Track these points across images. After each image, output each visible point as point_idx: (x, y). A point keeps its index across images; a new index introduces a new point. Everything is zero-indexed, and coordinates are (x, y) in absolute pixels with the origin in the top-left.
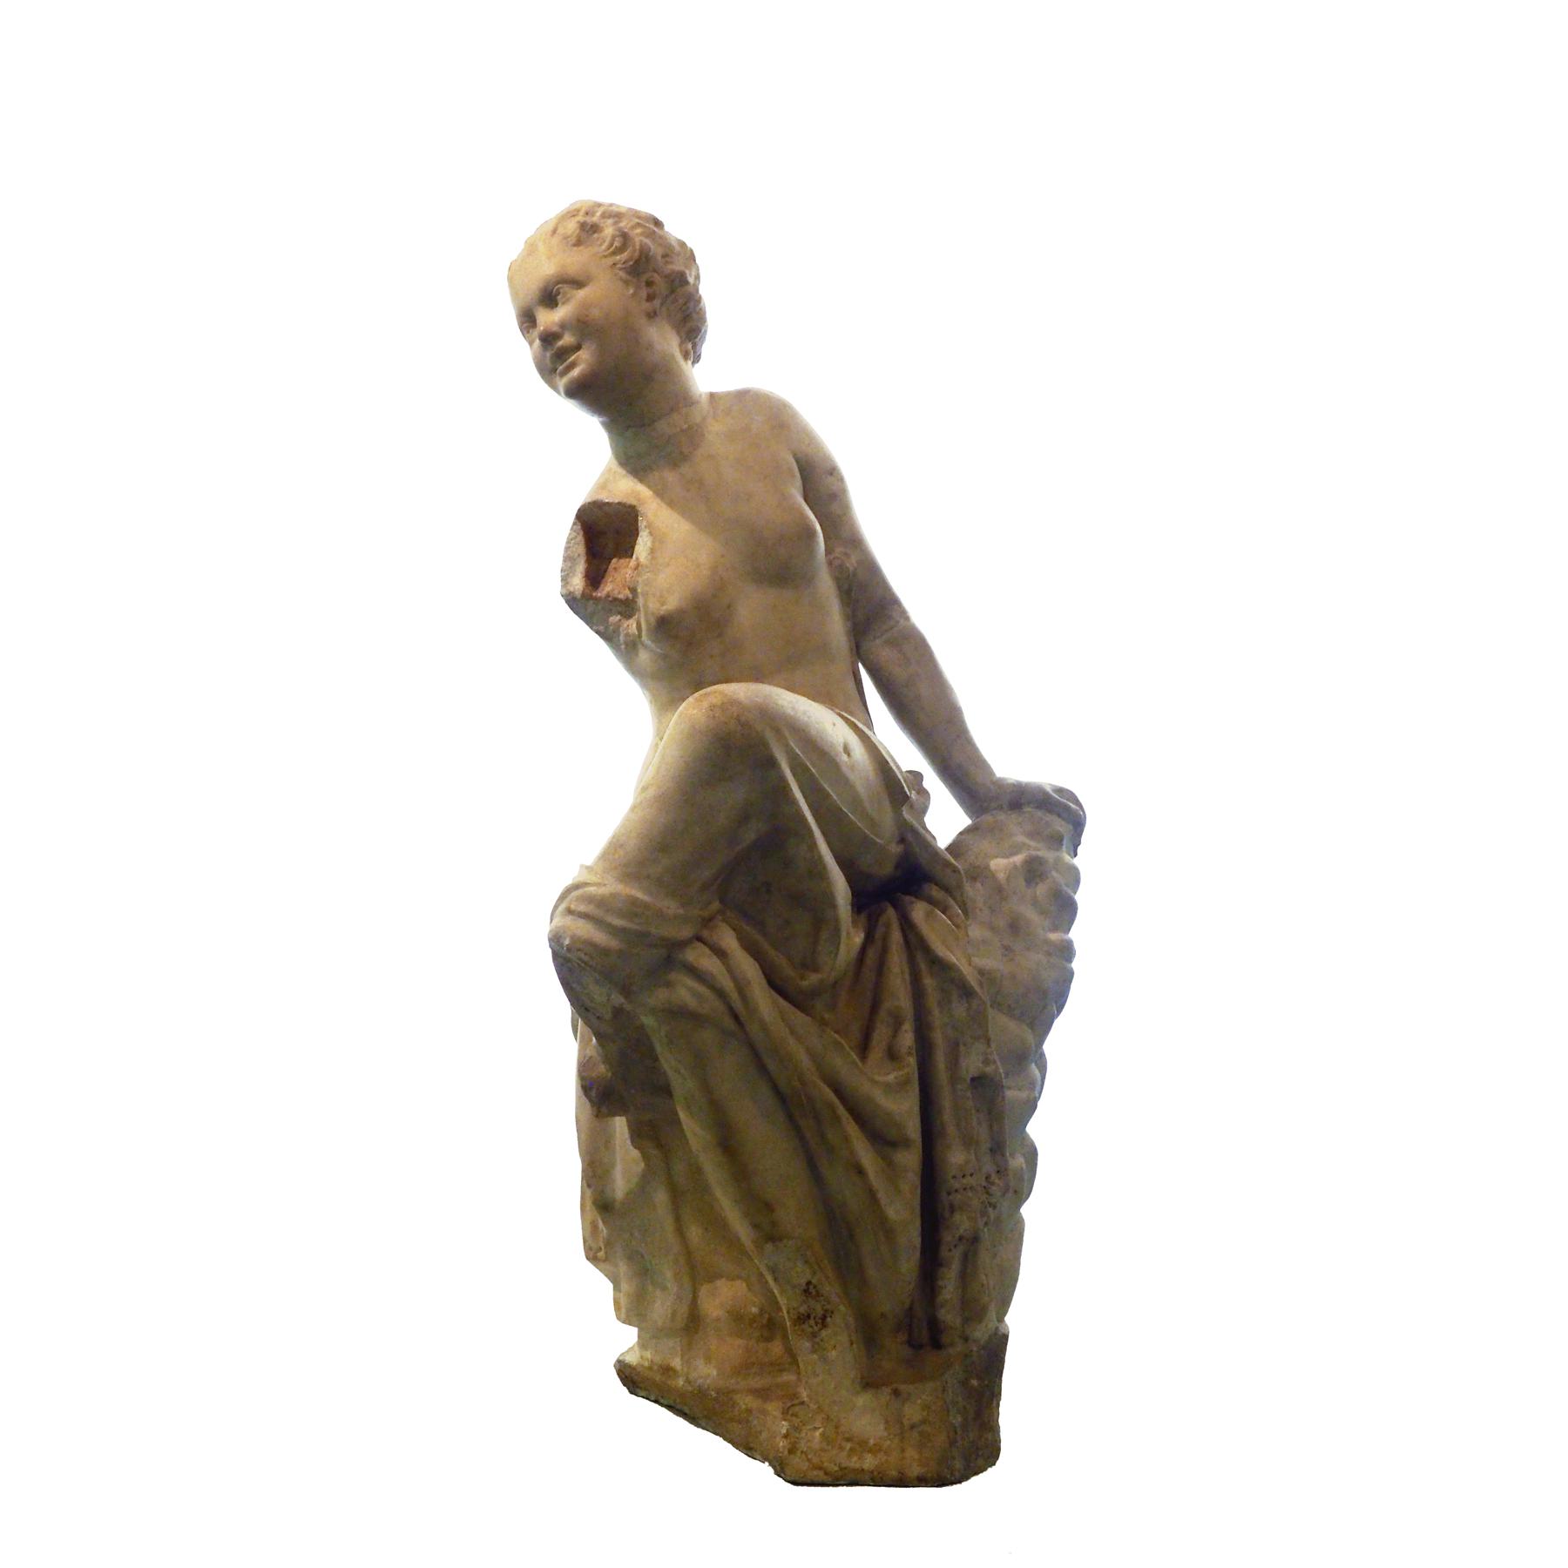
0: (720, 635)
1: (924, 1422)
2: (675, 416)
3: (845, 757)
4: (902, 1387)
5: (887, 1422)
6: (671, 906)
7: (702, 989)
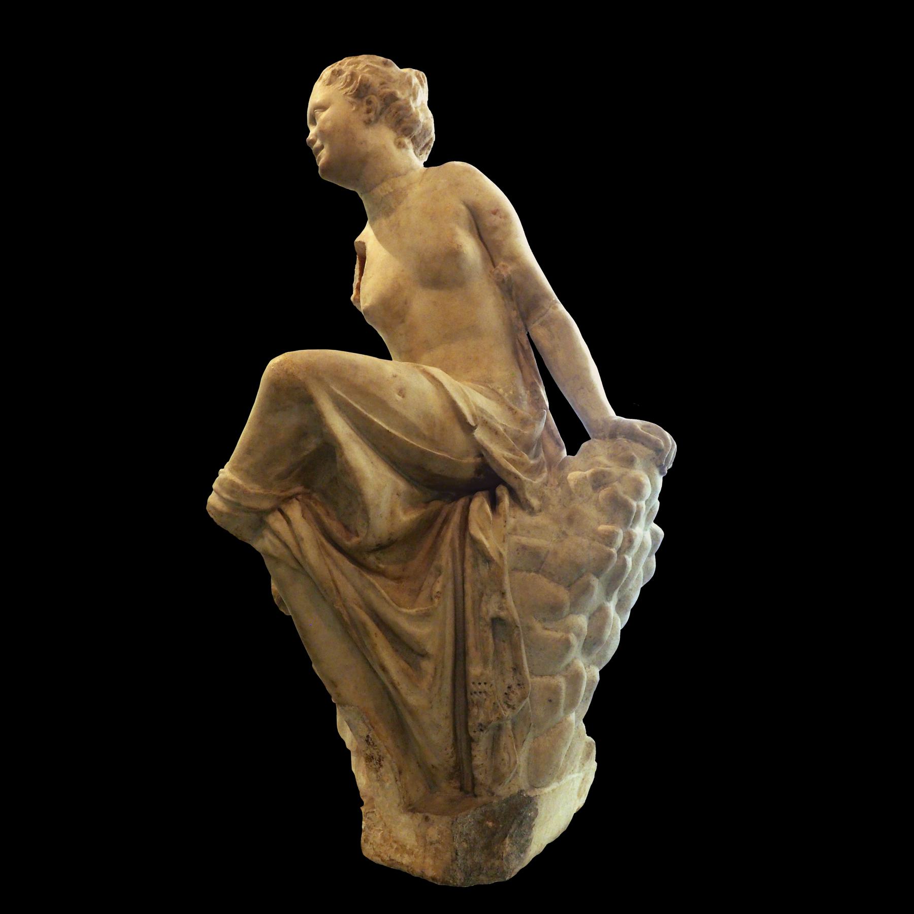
0: (403, 321)
1: (438, 842)
2: (385, 184)
3: (399, 398)
4: (432, 817)
5: (417, 835)
6: (254, 488)
7: (276, 541)
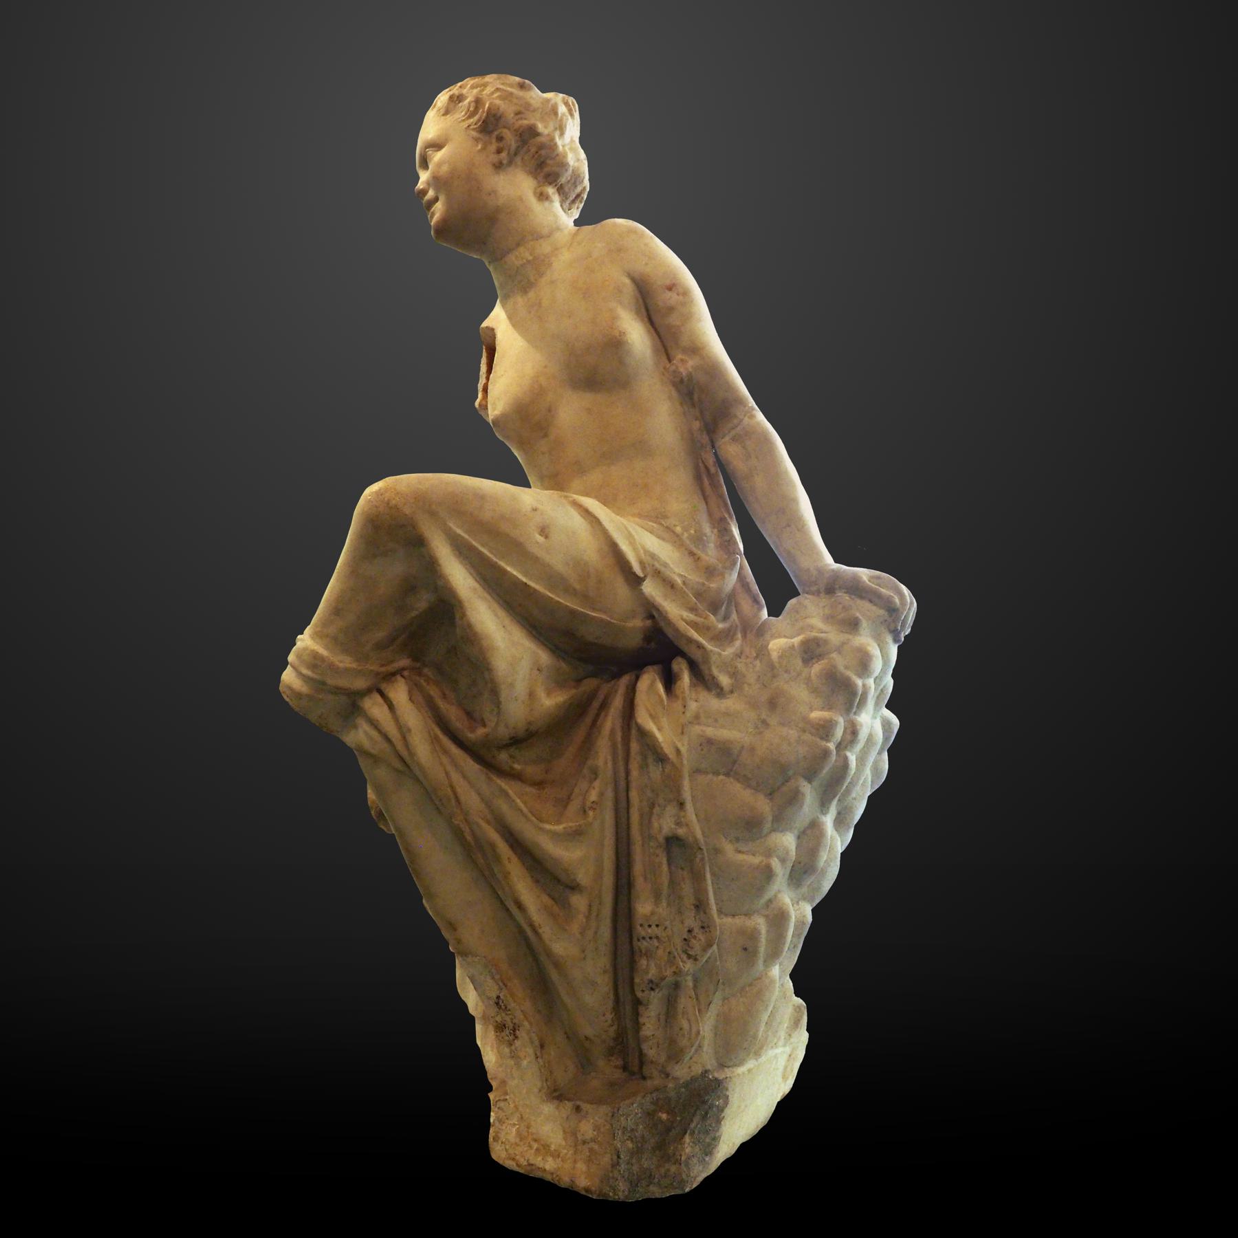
0: (546, 435)
1: (593, 1140)
2: (521, 249)
4: (586, 1107)
5: (564, 1132)
6: (344, 661)
7: (374, 733)
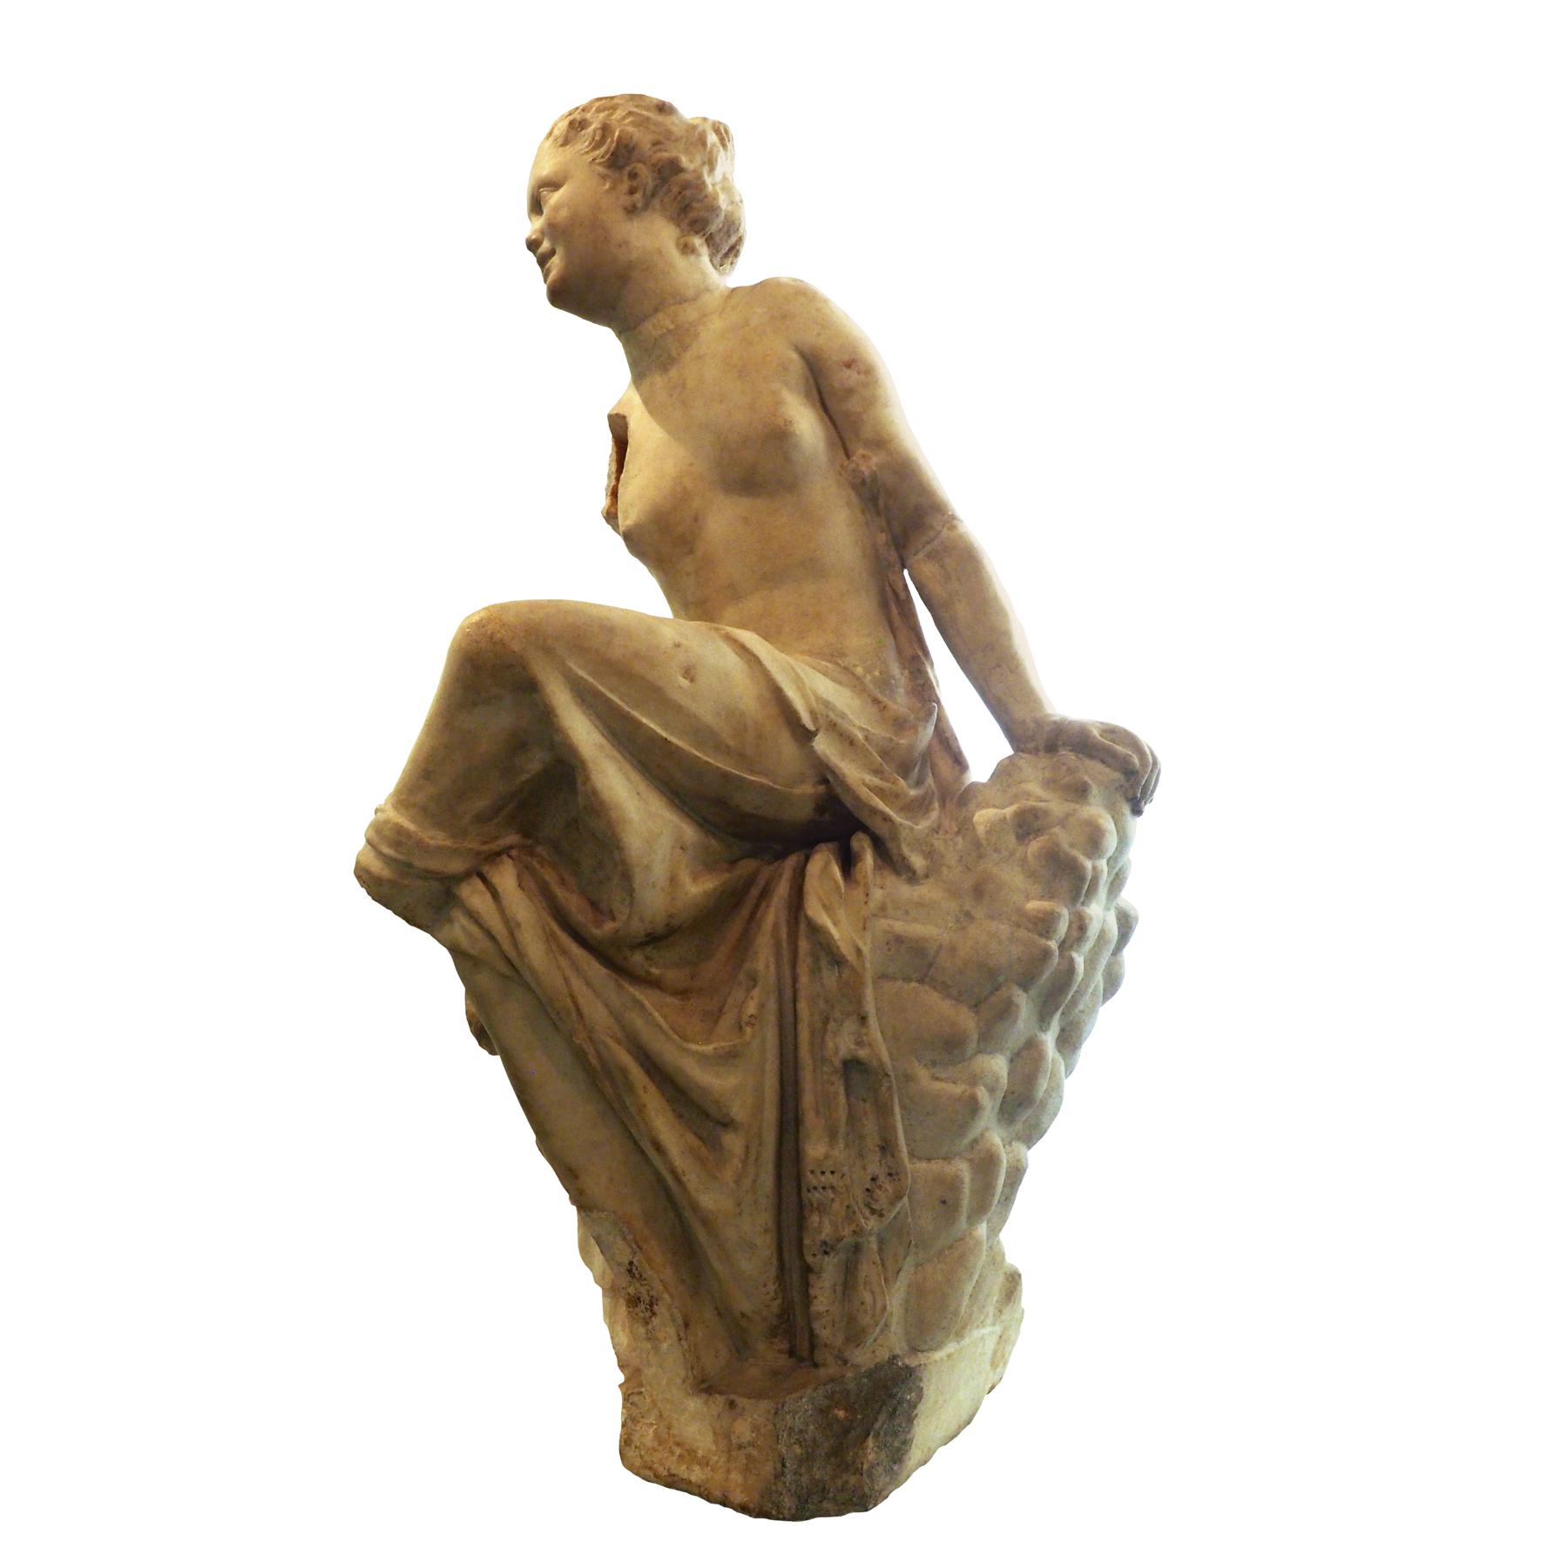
0: (691, 551)
1: (752, 1444)
2: (660, 316)
4: (742, 1402)
5: (715, 1433)
6: (436, 838)
7: (474, 929)
